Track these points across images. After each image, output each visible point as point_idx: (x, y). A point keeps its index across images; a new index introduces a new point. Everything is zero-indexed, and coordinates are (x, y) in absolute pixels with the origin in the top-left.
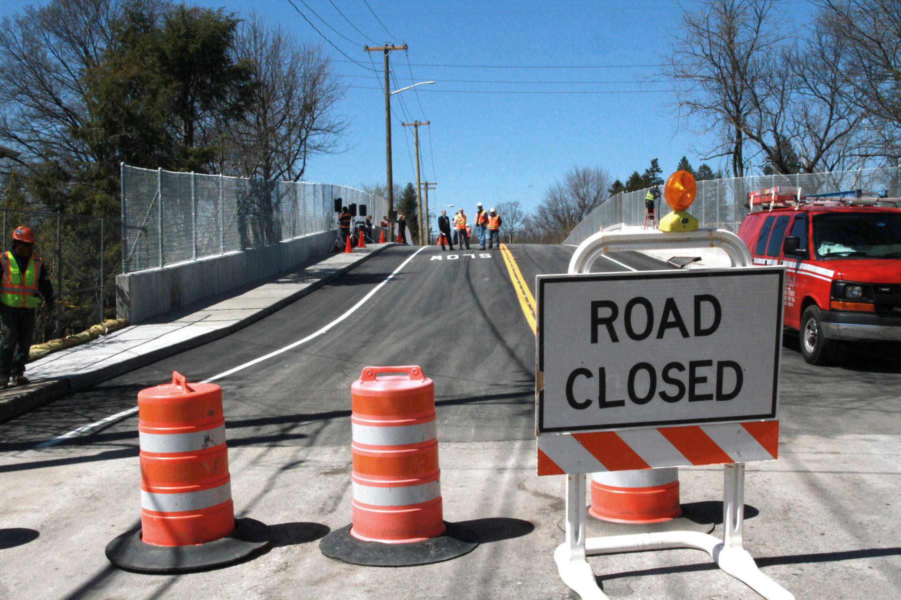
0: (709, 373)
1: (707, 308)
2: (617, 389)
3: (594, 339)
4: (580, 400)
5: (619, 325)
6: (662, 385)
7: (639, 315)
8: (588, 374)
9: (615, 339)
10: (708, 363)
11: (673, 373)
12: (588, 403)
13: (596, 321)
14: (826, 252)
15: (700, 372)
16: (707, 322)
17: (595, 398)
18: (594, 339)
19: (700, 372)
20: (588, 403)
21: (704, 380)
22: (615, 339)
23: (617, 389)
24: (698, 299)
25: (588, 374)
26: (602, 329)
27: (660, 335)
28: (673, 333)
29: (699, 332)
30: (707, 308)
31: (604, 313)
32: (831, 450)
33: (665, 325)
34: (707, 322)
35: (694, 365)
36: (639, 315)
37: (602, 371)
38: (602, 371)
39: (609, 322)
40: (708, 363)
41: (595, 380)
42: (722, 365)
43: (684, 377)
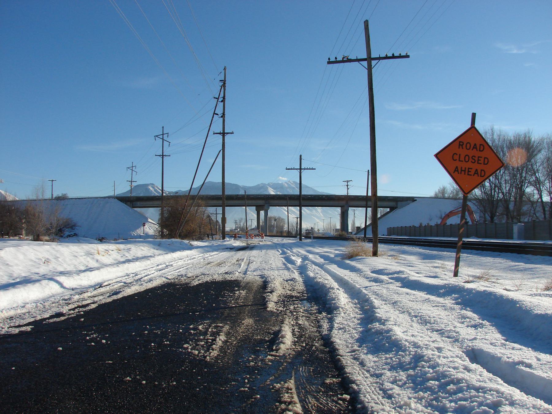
0: (482, 159)
1: (483, 172)
2: (462, 159)
3: (459, 148)
4: (455, 159)
5: (464, 146)
6: (471, 160)
7: (468, 145)
8: (457, 154)
9: (463, 148)
10: (481, 157)
11: (474, 158)
12: (456, 160)
13: (460, 145)
14: (488, 184)
15: (480, 159)
16: (481, 149)
17: (458, 159)
18: (459, 148)
19: (480, 159)
20: (456, 160)
21: (480, 160)
22: (463, 148)
23: (462, 159)
24: (482, 170)
25: (457, 154)
26: (461, 146)
27: (472, 150)
28: (475, 150)
29: (480, 151)
30: (483, 172)
31: (461, 144)
32: (154, 274)
33: (474, 148)
34: (481, 149)
35: (479, 157)
36: (468, 145)
37: (460, 155)
38: (460, 155)
39: (462, 145)
40: (481, 157)
41: (459, 155)
42: (485, 158)
43: (476, 159)
